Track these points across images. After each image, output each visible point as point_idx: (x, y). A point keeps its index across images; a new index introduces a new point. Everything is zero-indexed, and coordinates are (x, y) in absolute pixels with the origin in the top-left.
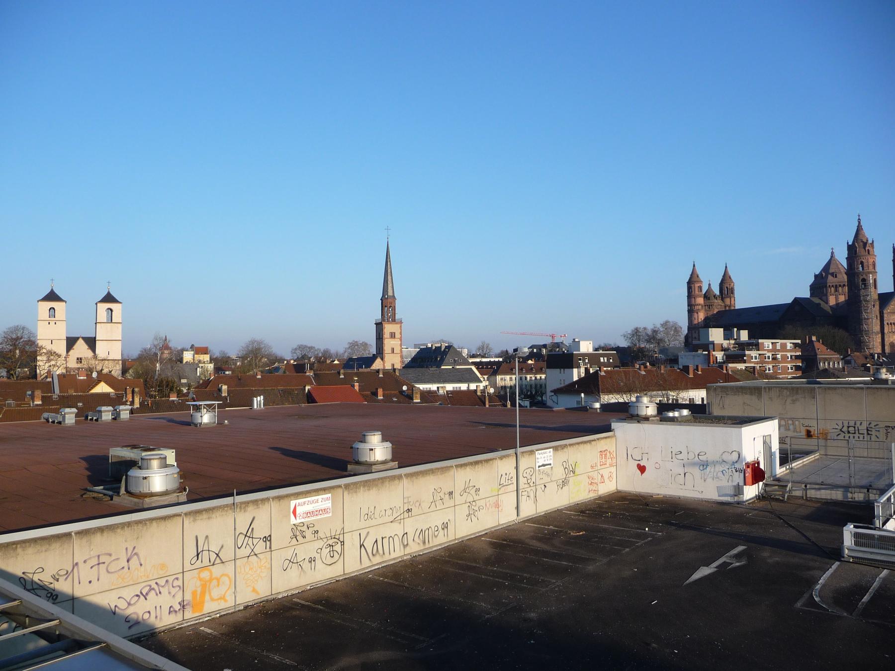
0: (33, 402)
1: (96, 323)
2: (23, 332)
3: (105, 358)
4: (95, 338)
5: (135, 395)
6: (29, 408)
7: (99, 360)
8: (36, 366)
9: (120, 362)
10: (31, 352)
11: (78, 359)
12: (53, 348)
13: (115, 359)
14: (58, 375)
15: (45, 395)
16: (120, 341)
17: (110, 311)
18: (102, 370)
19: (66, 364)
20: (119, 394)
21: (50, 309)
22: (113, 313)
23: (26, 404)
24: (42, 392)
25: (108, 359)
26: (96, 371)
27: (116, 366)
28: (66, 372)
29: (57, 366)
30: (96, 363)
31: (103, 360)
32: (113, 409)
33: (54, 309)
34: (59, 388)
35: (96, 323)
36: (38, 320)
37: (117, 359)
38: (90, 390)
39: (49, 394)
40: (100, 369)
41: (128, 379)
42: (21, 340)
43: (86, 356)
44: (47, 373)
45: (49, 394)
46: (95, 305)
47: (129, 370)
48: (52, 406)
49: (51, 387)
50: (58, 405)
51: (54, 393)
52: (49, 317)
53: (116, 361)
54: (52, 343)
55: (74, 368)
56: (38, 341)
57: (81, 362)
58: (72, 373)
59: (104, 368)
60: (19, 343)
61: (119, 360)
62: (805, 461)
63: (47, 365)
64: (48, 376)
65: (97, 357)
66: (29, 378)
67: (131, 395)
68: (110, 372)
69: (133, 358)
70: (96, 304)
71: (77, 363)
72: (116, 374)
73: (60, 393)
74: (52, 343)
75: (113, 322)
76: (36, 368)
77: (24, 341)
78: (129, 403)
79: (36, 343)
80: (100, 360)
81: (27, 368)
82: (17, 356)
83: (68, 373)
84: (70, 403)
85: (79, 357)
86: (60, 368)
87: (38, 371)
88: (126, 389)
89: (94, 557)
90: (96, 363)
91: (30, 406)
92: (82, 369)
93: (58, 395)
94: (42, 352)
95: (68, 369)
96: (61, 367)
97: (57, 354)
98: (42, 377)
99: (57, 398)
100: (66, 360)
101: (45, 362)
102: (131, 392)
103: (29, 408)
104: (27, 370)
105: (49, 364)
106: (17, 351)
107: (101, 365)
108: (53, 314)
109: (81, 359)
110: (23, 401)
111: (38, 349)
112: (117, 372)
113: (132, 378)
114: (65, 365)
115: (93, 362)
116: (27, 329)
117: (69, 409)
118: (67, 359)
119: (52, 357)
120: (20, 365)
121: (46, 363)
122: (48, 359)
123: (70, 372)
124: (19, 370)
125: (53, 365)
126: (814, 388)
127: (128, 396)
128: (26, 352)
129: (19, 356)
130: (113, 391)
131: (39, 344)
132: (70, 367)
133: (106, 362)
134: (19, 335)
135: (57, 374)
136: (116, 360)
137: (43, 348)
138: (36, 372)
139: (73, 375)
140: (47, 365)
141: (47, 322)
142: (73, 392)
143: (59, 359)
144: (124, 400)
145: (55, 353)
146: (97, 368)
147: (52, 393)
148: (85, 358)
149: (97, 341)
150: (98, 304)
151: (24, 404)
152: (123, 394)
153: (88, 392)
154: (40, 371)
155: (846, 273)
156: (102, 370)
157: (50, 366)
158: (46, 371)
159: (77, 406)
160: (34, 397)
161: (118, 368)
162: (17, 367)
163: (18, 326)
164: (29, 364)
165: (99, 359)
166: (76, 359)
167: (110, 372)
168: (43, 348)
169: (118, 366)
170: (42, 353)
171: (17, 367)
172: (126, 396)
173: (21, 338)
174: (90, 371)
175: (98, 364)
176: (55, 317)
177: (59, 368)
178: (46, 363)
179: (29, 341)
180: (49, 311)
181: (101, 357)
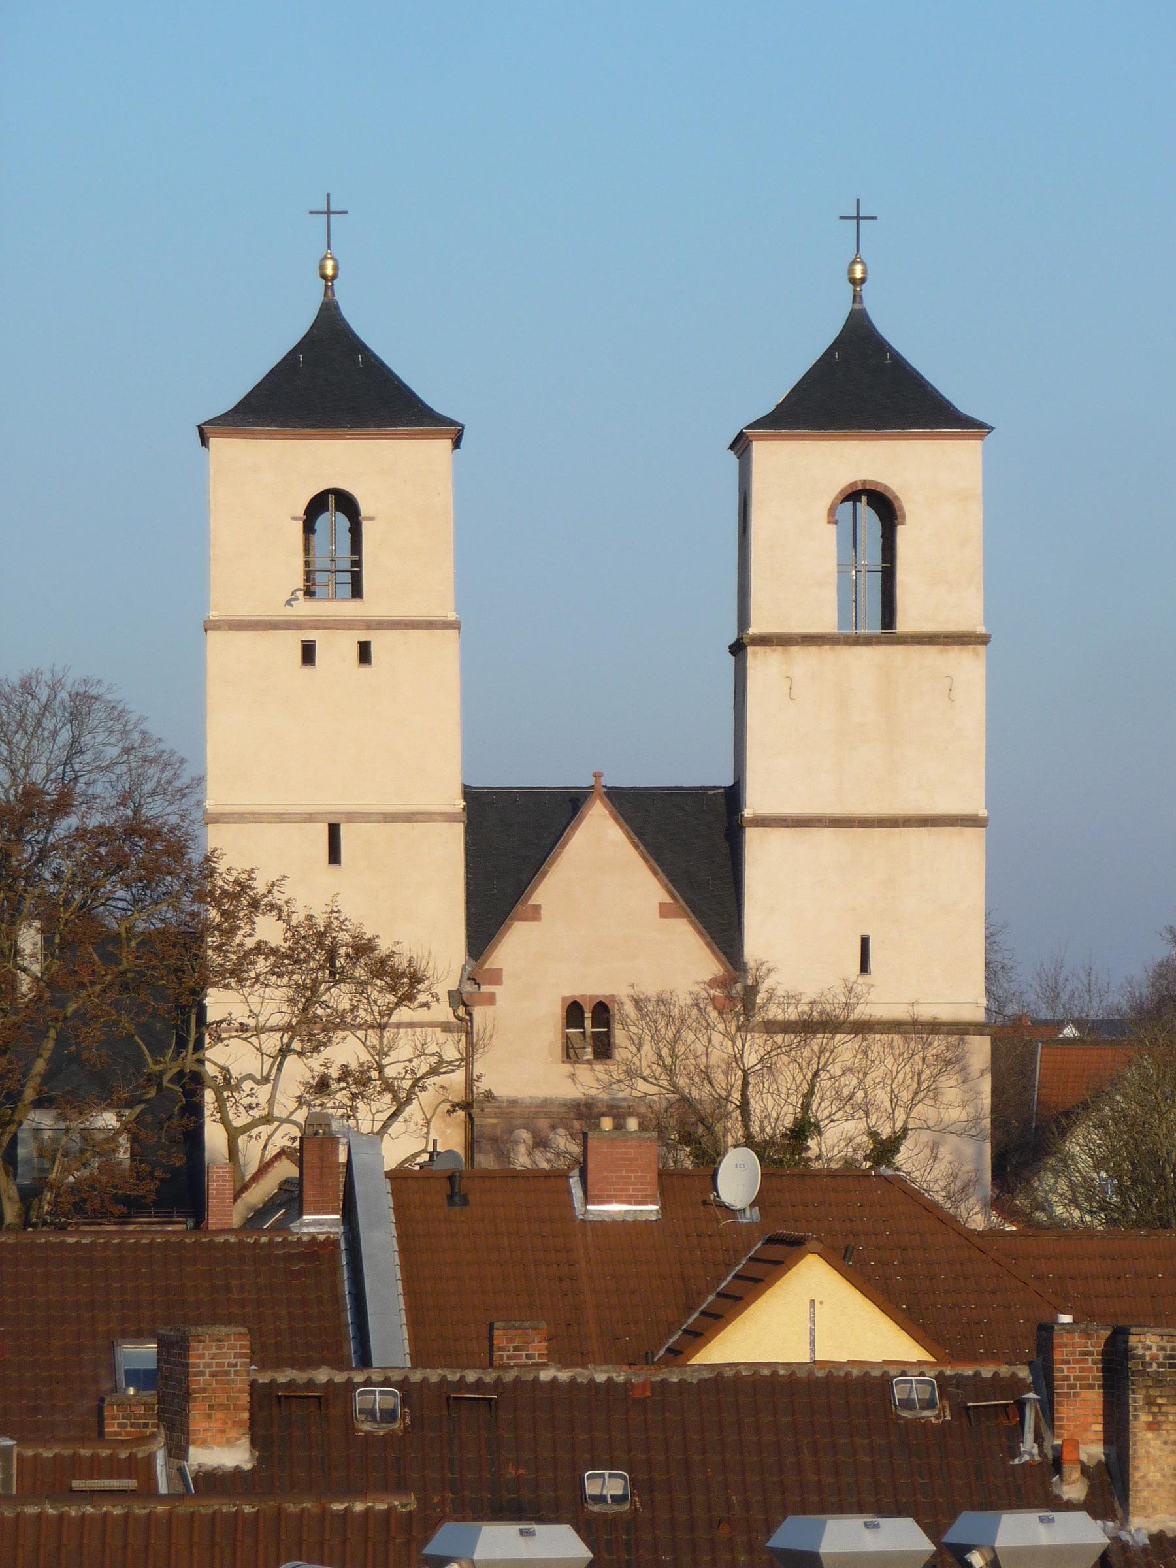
0: (177, 1451)
1: (738, 649)
2: (75, 748)
3: (834, 1004)
4: (733, 796)
5: (1137, 1398)
6: (140, 1511)
7: (771, 1027)
8: (194, 1082)
9: (980, 1050)
10: (147, 940)
11: (574, 1012)
12: (347, 911)
13: (926, 1012)
14: (398, 1177)
15: (283, 1377)
16: (974, 838)
17: (868, 518)
18: (803, 1129)
19: (468, 1059)
20: (978, 1385)
21: (317, 506)
22: (903, 534)
23: (114, 1468)
24: (261, 1355)
25: (860, 1012)
26: (748, 1141)
27: (936, 1093)
28: (471, 1145)
29: (388, 1086)
30: (751, 1059)
31: (807, 1027)
32: (924, 1544)
33: (346, 503)
34: (409, 1293)
35: (738, 649)
36: (209, 626)
37: (945, 1014)
38: (699, 1336)
39: (322, 1375)
40: (788, 1122)
41: (1056, 1225)
42: (68, 824)
43: (650, 989)
44: (298, 1156)
45: (322, 1375)
46: (732, 460)
47: (1063, 1133)
48: (353, 1491)
49: (337, 1299)
50: (400, 1487)
51: (365, 1361)
52: (309, 593)
53: (938, 1044)
54: (334, 856)
55: (543, 1107)
56: (216, 838)
57: (603, 1049)
58: (522, 1160)
59: (821, 1109)
60: (42, 856)
61: (961, 1029)
62: (128, 1348)
63: (297, 1072)
64: (309, 1194)
65: (751, 992)
66: (131, 1207)
67: (1095, 1397)
68: (885, 1149)
69: (1096, 1011)
70: (741, 445)
71: (570, 1053)
72: (940, 1170)
73: (419, 1358)
74: (334, 856)
75: (905, 623)
76: (195, 1110)
77: (81, 834)
78: (1074, 1489)
79: (194, 856)
80: (786, 1027)
81: (117, 1106)
82: (25, 985)
83: (486, 1161)
84: (511, 1471)
85: (590, 988)
86: (412, 1110)
87: (214, 1136)
88: (1046, 1332)
89: (450, 1101)
90: (751, 1059)
91: (148, 1490)
92: (619, 1112)
93: (404, 1385)
94: (245, 939)
95: (488, 1121)
96: (425, 1098)
97: (382, 968)
98: (257, 1195)
99: (389, 1415)
100: (465, 1026)
101: (272, 1042)
102: (1095, 1373)
103: (140, 1511)
104: (108, 1119)
105: (315, 1062)
106: (29, 939)
107: (791, 1078)
108: (344, 557)
109: (602, 1011)
110: (83, 1441)
111: (214, 915)
112: (945, 1152)
113: (1097, 1222)
114: (458, 1077)
115: (721, 1048)
116: (116, 713)
117: (509, 1530)
118: (478, 1012)
119: (339, 997)
120: (47, 1078)
121: (284, 1051)
122: (306, 1018)
123: (501, 1146)
124: (45, 1120)
125: (345, 1073)
126: (375, 1390)
127: (1065, 1410)
128: (109, 944)
129: (48, 983)
130: (925, 1356)
131: (221, 867)
132: (503, 1091)
133: (846, 1048)
134: (38, 773)
135: (390, 1163)
136: (934, 1027)
137: (254, 905)
138: (194, 1139)
139: (534, 1176)
140: (297, 1072)
141: (292, 642)
142: (537, 1348)
143: (403, 1014)
144: (1029, 1447)
145: (363, 948)
146: (755, 1105)
147: (340, 1364)
148: (637, 1002)
149: (753, 838)
150: (762, 451)
151: (97, 1468)
152: (1015, 1384)
153: (677, 1354)
154: (233, 1135)
155: (663, 1380)
156: (803, 1129)
157: (322, 1086)
158: (284, 1137)
159: (581, 1496)
160: (186, 1397)
161: (957, 1115)
162: (29, 1094)
163: (27, 688)
164: (140, 1063)
165: (774, 1012)
166: (557, 1012)
167: (885, 1149)
168: (254, 905)
169: (951, 1090)
170: (247, 957)
171: (29, 1094)
172: (1048, 1410)
173: (62, 806)
174: (687, 1139)
175: (768, 1065)
176: (357, 592)
177: (400, 1107)
178: (284, 1051)
179: (134, 829)
180: (309, 528)
181: (792, 998)
